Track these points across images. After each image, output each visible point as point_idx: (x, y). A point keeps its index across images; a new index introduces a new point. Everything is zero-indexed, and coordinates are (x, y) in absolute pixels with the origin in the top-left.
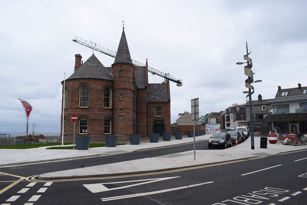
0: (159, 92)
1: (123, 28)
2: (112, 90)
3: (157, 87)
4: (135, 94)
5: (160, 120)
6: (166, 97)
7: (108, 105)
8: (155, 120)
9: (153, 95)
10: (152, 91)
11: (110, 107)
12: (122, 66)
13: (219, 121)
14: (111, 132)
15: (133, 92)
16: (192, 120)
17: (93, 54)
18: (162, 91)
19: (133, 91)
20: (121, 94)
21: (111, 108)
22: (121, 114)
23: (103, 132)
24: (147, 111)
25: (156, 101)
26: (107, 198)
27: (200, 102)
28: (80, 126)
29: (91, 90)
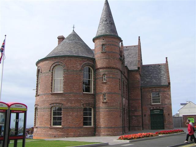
0: (156, 74)
2: (93, 70)
4: (125, 77)
5: (158, 108)
7: (88, 90)
8: (152, 109)
9: (148, 78)
10: (147, 73)
12: (104, 39)
13: (17, 117)
15: (121, 72)
16: (145, 115)
17: (73, 31)
19: (120, 70)
21: (92, 93)
23: (82, 124)
24: (141, 98)
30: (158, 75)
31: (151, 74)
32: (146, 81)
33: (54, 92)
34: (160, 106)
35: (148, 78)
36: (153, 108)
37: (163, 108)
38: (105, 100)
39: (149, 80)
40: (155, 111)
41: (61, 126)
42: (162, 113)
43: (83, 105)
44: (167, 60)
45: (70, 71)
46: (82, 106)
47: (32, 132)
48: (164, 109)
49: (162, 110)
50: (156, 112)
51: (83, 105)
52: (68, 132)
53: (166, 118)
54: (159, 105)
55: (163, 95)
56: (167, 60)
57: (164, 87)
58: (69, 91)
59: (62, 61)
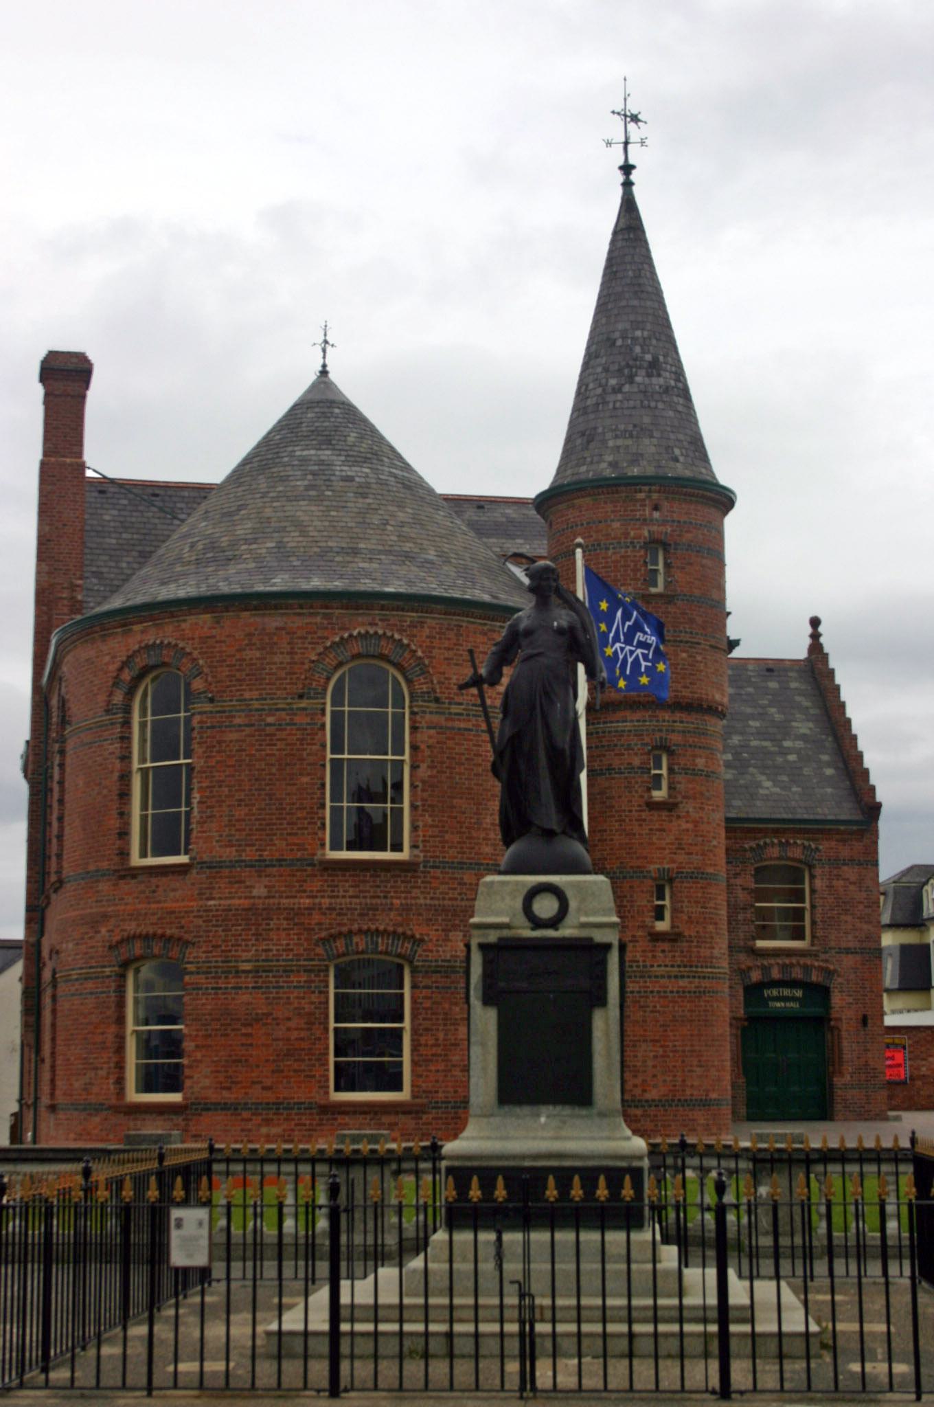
0: (761, 734)
5: (797, 974)
8: (755, 976)
12: (665, 505)
22: (662, 926)
33: (143, 854)
36: (765, 969)
37: (830, 973)
40: (775, 992)
41: (175, 1097)
42: (815, 1011)
45: (455, 709)
48: (836, 984)
49: (820, 993)
50: (784, 1002)
57: (838, 832)
58: (452, 852)
59: (401, 631)
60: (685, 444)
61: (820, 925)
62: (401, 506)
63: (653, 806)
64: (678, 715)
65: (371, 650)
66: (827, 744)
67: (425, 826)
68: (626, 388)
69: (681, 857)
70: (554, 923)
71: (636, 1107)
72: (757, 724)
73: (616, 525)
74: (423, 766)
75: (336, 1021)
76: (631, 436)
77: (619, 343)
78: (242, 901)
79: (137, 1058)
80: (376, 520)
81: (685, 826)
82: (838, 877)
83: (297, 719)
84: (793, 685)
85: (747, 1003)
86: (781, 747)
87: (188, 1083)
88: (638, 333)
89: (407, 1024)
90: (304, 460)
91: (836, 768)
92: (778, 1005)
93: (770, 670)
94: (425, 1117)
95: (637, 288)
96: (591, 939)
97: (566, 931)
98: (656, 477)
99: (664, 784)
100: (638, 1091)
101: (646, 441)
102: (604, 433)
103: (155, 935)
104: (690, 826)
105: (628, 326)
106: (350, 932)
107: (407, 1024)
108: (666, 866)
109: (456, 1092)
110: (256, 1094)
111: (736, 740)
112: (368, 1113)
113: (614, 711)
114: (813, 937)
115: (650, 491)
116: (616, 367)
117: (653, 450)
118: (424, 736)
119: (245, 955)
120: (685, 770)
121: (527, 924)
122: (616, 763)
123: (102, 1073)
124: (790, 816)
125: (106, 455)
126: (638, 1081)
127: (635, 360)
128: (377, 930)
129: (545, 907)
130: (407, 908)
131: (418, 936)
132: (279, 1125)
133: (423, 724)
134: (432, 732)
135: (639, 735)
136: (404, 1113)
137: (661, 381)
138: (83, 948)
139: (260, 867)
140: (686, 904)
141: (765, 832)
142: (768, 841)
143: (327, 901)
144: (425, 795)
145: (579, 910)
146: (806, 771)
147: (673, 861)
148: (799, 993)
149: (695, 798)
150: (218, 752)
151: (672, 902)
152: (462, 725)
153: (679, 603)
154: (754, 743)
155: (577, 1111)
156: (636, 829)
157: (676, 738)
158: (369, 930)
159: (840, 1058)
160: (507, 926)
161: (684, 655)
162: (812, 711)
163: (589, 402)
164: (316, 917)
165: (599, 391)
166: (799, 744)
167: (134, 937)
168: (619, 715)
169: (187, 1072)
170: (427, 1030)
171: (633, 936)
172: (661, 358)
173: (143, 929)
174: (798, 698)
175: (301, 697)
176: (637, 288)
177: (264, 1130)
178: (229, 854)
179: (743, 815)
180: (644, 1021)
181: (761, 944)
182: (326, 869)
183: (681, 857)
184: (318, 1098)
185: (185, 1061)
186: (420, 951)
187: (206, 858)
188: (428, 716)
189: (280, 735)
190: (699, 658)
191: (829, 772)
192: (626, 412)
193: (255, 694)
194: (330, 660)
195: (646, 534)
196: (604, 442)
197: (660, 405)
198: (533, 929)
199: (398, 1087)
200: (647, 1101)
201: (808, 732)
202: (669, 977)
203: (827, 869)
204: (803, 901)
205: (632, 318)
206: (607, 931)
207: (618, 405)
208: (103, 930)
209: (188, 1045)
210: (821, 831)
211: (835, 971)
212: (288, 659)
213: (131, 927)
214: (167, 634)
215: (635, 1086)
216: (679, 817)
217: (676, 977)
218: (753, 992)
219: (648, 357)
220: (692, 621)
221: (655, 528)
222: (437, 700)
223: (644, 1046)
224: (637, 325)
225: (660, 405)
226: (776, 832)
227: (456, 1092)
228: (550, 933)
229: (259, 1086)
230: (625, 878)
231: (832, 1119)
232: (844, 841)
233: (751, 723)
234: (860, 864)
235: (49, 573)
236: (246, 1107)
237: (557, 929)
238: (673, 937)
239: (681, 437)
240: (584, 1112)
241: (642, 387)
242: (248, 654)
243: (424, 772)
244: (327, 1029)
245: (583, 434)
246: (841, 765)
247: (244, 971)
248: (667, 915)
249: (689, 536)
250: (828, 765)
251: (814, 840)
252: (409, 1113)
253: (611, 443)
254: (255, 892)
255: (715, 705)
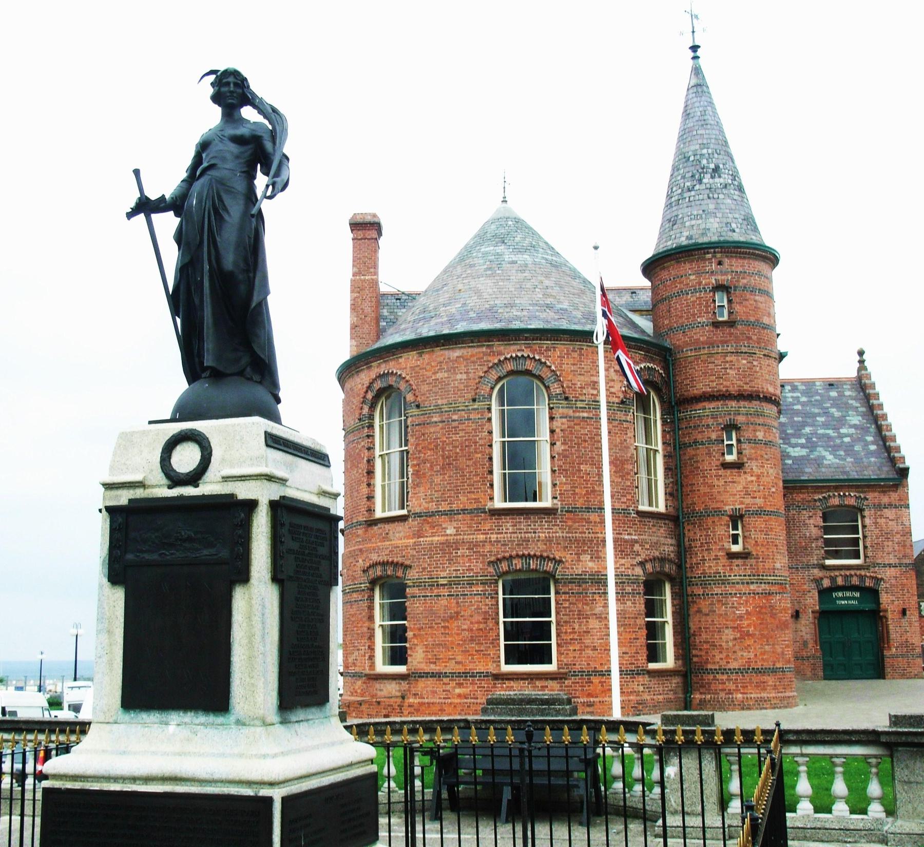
0: (825, 425)
1: (694, 48)
3: (804, 399)
5: (855, 581)
6: (872, 453)
8: (826, 583)
9: (793, 441)
11: (657, 506)
12: (726, 261)
14: (677, 658)
18: (842, 421)
20: (731, 427)
22: (736, 548)
25: (825, 473)
26: (38, 830)
27: (109, 479)
28: (550, 616)
29: (566, 399)
30: (836, 429)
31: (804, 424)
32: (789, 457)
33: (384, 511)
34: (863, 573)
35: (793, 441)
36: (833, 579)
37: (878, 580)
38: (735, 542)
39: (804, 452)
40: (840, 594)
42: (868, 607)
43: (642, 564)
44: (861, 362)
45: (579, 404)
46: (638, 571)
47: (84, 732)
49: (872, 593)
50: (846, 600)
51: (642, 564)
52: (590, 695)
53: (891, 627)
54: (858, 567)
55: (876, 523)
56: (861, 362)
59: (540, 353)
60: (740, 220)
61: (870, 549)
62: (547, 276)
63: (726, 466)
64: (742, 403)
65: (520, 368)
66: (871, 430)
67: (561, 483)
68: (697, 187)
69: (748, 500)
70: (194, 478)
71: (723, 673)
72: (823, 419)
73: (692, 277)
74: (558, 443)
75: (504, 617)
76: (701, 218)
77: (692, 158)
78: (439, 538)
79: (384, 642)
80: (529, 285)
81: (750, 479)
82: (881, 516)
83: (472, 416)
84: (847, 393)
85: (821, 602)
86: (839, 433)
87: (409, 659)
88: (705, 151)
89: (553, 618)
90: (485, 254)
91: (877, 445)
92: (843, 602)
93: (831, 385)
94: (566, 682)
95: (703, 122)
96: (232, 496)
97: (209, 487)
98: (719, 242)
99: (735, 450)
100: (723, 663)
101: (712, 220)
102: (683, 218)
103: (388, 561)
104: (754, 478)
105: (697, 147)
106: (511, 556)
107: (553, 618)
108: (738, 507)
109: (588, 664)
110: (451, 667)
111: (808, 430)
112: (527, 679)
113: (697, 402)
114: (866, 557)
115: (715, 252)
116: (690, 174)
117: (716, 225)
118: (557, 424)
119: (443, 574)
120: (749, 441)
121: (165, 481)
122: (699, 437)
123: (362, 652)
124: (846, 477)
125: (392, 276)
126: (723, 655)
127: (703, 168)
128: (529, 555)
129: (186, 459)
130: (549, 540)
131: (557, 558)
132: (467, 687)
133: (558, 416)
134: (564, 420)
135: (714, 417)
136: (552, 679)
137: (722, 180)
138: (350, 572)
139: (450, 514)
140: (753, 532)
141: (829, 488)
142: (831, 494)
143: (495, 536)
144: (561, 463)
145: (223, 460)
146: (857, 448)
147: (742, 503)
148: (857, 595)
149: (757, 459)
150: (423, 440)
151: (743, 532)
152: (585, 415)
153: (739, 327)
154: (821, 431)
155: (211, 718)
156: (716, 482)
157: (741, 419)
158: (523, 555)
159: (888, 637)
160: (141, 485)
161: (744, 362)
162: (861, 409)
163: (673, 199)
164: (488, 548)
165: (680, 191)
166: (852, 431)
167: (376, 564)
168: (701, 405)
169: (409, 652)
170: (565, 622)
171: (716, 556)
172: (721, 166)
173: (381, 559)
174: (850, 402)
175: (474, 400)
176: (703, 122)
177: (458, 691)
178: (433, 507)
179: (811, 478)
180: (726, 614)
181: (829, 562)
182: (493, 515)
183: (748, 500)
184: (492, 668)
185: (407, 645)
186: (559, 569)
187: (418, 510)
188: (561, 410)
189: (461, 427)
190: (755, 363)
191: (873, 447)
192: (698, 203)
193: (445, 401)
194: (494, 375)
195: (714, 282)
196: (683, 223)
197: (721, 196)
198: (170, 487)
199: (550, 662)
200: (730, 669)
201: (858, 423)
202: (743, 583)
203: (873, 512)
204: (858, 534)
205: (700, 141)
206: (252, 484)
207: (692, 199)
208: (360, 561)
209: (409, 634)
210: (868, 486)
211: (882, 579)
212: (464, 376)
213: (375, 558)
214: (390, 366)
215: (721, 659)
216: (745, 473)
217: (748, 583)
218: (824, 594)
219: (712, 166)
220: (749, 338)
221: (719, 277)
222: (566, 399)
223: (726, 631)
224: (703, 146)
225: (721, 196)
226: (836, 488)
227: (588, 664)
228: (189, 491)
229: (454, 661)
230: (709, 516)
231: (884, 678)
232: (884, 492)
233: (818, 419)
234: (896, 507)
235: (357, 346)
236: (445, 675)
237: (197, 486)
238: (744, 555)
239: (737, 216)
240: (220, 719)
241: (708, 186)
242: (439, 375)
243: (559, 447)
244: (498, 623)
245: (669, 221)
246: (881, 443)
247: (442, 585)
248: (740, 540)
249: (745, 281)
250: (873, 443)
251: (862, 492)
252: (555, 679)
253: (687, 224)
254: (448, 532)
255: (768, 395)
